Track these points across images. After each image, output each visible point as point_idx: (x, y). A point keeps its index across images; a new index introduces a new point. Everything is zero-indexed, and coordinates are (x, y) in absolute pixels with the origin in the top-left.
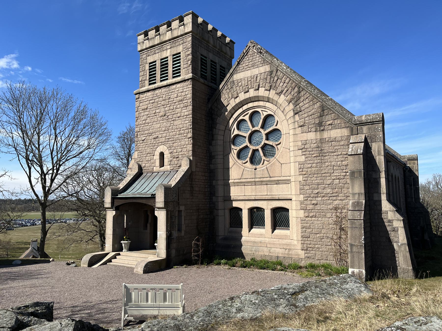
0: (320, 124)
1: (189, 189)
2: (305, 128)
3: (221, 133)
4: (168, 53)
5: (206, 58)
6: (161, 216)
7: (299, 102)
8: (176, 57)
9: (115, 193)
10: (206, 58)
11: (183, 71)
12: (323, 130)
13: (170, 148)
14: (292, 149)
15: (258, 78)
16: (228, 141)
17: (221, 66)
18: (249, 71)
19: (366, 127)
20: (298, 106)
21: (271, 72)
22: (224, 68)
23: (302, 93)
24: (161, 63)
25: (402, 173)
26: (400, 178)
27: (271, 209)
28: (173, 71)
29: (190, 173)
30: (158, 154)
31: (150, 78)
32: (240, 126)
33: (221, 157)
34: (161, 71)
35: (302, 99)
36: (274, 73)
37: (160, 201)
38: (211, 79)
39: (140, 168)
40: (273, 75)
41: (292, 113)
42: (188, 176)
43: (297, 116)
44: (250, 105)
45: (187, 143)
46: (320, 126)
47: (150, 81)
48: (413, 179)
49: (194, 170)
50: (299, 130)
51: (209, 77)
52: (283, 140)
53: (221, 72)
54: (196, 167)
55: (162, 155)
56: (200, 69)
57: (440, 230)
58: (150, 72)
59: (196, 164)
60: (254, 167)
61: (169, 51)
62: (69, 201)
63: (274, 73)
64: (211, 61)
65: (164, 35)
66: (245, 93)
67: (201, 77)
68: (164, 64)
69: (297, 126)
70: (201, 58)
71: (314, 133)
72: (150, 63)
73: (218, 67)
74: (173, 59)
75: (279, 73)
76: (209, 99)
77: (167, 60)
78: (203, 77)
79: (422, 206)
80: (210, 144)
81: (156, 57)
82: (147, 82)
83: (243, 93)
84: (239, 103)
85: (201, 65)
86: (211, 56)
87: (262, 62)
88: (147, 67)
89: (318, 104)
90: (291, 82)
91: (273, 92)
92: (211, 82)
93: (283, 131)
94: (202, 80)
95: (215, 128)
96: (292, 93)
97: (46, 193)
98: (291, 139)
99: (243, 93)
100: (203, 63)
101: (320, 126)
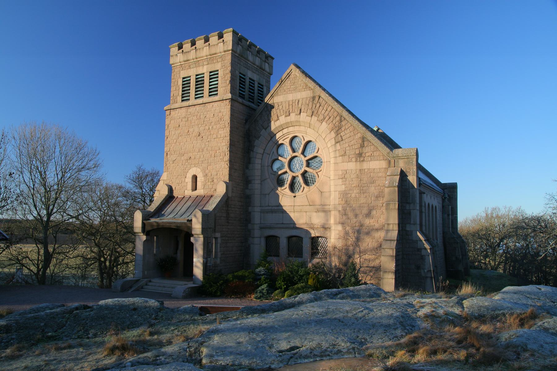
0: (360, 155)
1: (225, 215)
2: (346, 157)
3: (259, 156)
4: (205, 70)
5: (244, 75)
6: (198, 242)
7: (340, 131)
8: (214, 75)
9: (146, 217)
10: (244, 75)
11: (220, 90)
12: (363, 161)
13: (204, 171)
14: (332, 177)
15: (300, 103)
16: (267, 165)
17: (259, 84)
18: (291, 95)
19: (402, 160)
20: (339, 135)
21: (314, 98)
22: (262, 86)
23: (343, 123)
24: (196, 79)
25: (441, 202)
26: (437, 207)
27: (456, 183)
28: (210, 89)
29: (225, 199)
30: (191, 177)
31: (183, 94)
32: (293, 167)
33: (259, 182)
34: (194, 88)
35: (343, 129)
36: (317, 99)
37: (197, 226)
38: (249, 98)
39: (171, 190)
40: (315, 102)
41: (333, 142)
42: (226, 201)
43: (338, 145)
44: (291, 129)
45: (223, 166)
46: (360, 156)
47: (182, 97)
48: (452, 208)
49: (230, 195)
50: (340, 159)
51: (247, 96)
52: (324, 167)
53: (259, 90)
54: (232, 192)
55: (195, 178)
56: (238, 88)
57: (2, 150)
58: (183, 88)
59: (233, 189)
60: (293, 195)
61: (205, 67)
62: (71, 224)
63: (317, 99)
64: (250, 79)
65: (201, 50)
66: (286, 116)
67: (240, 96)
68: (199, 81)
69: (338, 155)
70: (240, 77)
71: (354, 163)
72: (184, 78)
73: (256, 85)
74: (210, 76)
75: (321, 100)
76: (246, 121)
77: (203, 77)
78: (242, 96)
79: (459, 236)
80: (247, 168)
81: (192, 73)
82: (179, 98)
83: (283, 116)
84: (279, 126)
85: (240, 83)
86: (250, 74)
87: (304, 87)
88: (180, 82)
89: (359, 135)
90: (332, 110)
91: (314, 118)
92: (249, 101)
93: (324, 159)
94: (240, 100)
95: (253, 151)
96: (334, 122)
97: (49, 215)
98: (332, 167)
99: (283, 116)
100: (242, 81)
101: (360, 156)
